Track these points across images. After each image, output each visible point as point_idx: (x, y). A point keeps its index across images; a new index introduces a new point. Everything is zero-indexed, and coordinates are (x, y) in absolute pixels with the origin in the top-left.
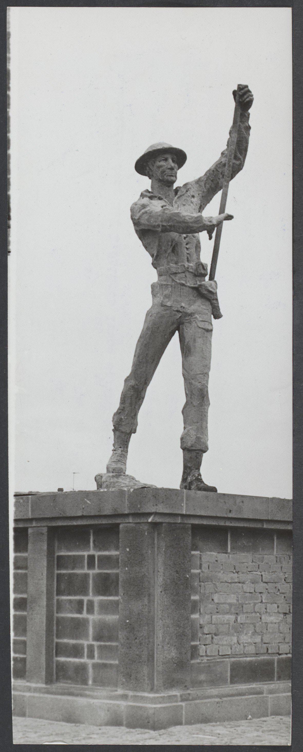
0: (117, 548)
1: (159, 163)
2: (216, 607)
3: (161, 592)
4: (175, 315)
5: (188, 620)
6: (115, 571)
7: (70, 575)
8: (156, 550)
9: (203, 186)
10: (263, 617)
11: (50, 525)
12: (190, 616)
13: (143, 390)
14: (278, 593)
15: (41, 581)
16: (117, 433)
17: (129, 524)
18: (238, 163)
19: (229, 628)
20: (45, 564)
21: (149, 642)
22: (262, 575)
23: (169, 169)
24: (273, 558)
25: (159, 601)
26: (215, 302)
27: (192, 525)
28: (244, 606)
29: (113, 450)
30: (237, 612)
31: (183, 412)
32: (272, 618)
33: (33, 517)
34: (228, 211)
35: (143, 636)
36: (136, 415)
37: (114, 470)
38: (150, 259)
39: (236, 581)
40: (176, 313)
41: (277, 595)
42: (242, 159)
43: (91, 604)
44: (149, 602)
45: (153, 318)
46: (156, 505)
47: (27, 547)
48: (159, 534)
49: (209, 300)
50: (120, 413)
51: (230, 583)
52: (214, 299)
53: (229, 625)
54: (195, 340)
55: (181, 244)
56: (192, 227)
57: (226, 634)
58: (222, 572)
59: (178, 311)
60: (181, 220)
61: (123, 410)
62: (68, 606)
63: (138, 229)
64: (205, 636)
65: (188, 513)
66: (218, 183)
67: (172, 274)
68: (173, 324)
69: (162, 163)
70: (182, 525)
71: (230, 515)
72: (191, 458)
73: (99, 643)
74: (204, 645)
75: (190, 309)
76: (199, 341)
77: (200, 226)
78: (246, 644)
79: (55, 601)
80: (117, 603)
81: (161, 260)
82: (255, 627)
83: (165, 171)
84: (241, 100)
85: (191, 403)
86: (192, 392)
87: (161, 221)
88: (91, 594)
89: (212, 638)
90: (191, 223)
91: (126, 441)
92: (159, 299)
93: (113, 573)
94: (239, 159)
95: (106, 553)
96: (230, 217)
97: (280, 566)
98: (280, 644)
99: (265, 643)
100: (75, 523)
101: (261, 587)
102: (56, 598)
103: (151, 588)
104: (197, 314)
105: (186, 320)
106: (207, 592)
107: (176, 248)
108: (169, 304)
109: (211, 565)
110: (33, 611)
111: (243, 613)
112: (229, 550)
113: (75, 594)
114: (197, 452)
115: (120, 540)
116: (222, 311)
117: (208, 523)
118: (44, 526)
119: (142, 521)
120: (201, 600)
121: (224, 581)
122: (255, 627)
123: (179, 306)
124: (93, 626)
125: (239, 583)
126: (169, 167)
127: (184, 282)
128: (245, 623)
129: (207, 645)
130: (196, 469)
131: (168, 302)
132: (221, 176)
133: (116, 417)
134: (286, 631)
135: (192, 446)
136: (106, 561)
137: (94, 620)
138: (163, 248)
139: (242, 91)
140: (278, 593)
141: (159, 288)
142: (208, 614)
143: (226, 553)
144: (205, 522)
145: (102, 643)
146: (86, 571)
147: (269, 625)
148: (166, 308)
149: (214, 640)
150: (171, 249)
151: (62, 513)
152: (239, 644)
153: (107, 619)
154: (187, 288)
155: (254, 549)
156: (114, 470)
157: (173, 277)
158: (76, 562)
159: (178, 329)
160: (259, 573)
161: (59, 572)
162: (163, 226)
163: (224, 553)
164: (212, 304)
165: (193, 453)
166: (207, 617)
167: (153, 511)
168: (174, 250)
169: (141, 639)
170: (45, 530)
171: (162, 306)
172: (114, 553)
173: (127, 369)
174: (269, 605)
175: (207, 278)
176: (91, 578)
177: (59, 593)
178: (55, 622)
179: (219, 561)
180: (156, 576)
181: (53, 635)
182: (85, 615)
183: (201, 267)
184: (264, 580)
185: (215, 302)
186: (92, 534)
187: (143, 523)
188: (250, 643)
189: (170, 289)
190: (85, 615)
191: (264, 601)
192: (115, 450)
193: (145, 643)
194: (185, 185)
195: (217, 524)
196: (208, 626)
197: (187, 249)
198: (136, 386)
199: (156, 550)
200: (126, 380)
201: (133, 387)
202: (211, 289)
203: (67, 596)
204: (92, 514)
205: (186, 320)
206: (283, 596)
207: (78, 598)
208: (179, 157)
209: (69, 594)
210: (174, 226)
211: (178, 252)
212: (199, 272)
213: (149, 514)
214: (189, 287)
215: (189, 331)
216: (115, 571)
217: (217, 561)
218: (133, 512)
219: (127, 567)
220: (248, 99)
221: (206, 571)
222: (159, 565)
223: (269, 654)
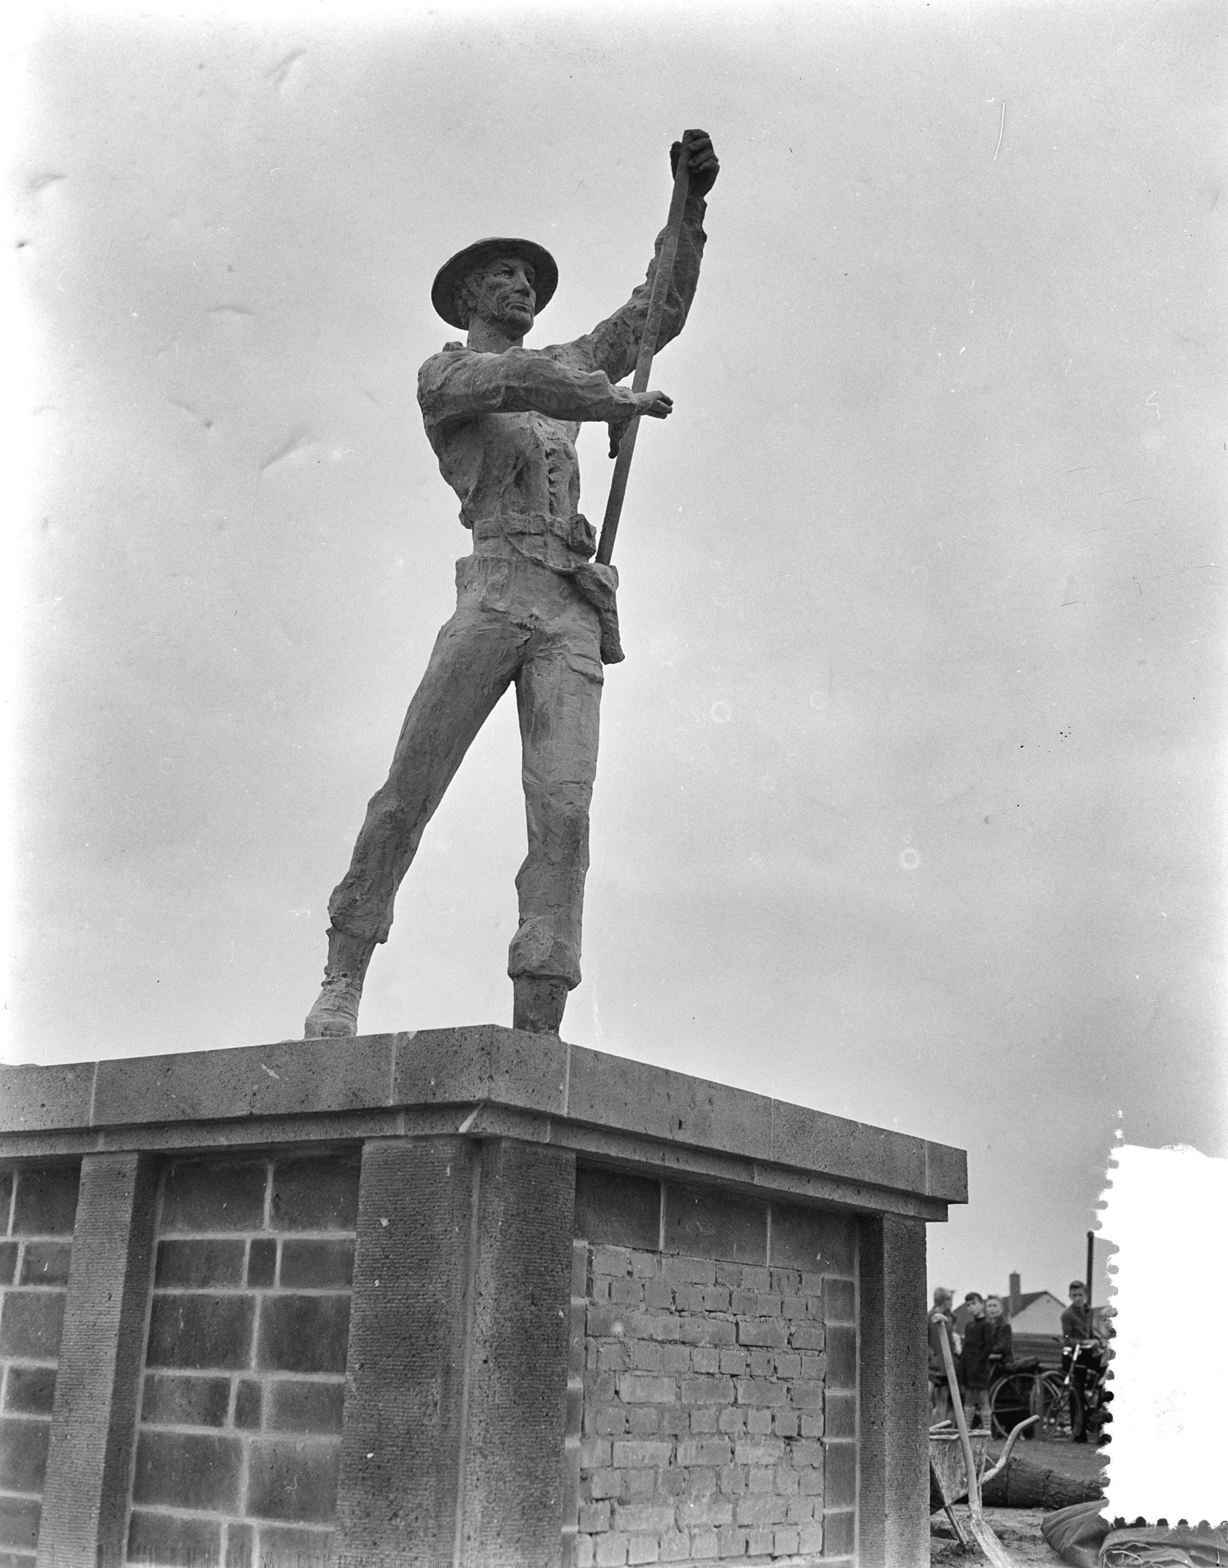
0: (347, 1221)
1: (492, 281)
2: (624, 1413)
3: (485, 1362)
4: (514, 635)
5: (557, 1454)
6: (333, 1292)
7: (193, 1299)
8: (474, 1226)
9: (591, 353)
10: (738, 1449)
11: (147, 1147)
12: (563, 1442)
13: (415, 825)
14: (774, 1379)
15: (104, 1319)
16: (340, 938)
17: (392, 1143)
18: (673, 311)
19: (656, 1480)
20: (122, 1265)
21: (440, 1526)
22: (737, 1324)
23: (517, 292)
24: (762, 1275)
25: (477, 1393)
26: (609, 616)
27: (582, 1156)
28: (695, 1414)
29: (323, 984)
30: (677, 1432)
31: (518, 883)
32: (760, 1451)
33: (98, 1123)
35: (420, 1505)
36: (391, 892)
37: (326, 1029)
38: (456, 505)
39: (677, 1337)
40: (518, 631)
41: (771, 1383)
42: (683, 305)
43: (250, 1394)
44: (445, 1396)
45: (458, 639)
46: (491, 1077)
47: (74, 1210)
48: (485, 1175)
49: (597, 610)
50: (352, 884)
51: (662, 1342)
52: (608, 610)
53: (657, 1473)
54: (560, 700)
55: (539, 467)
56: (582, 398)
57: (649, 1500)
58: (643, 1306)
59: (522, 626)
60: (556, 377)
61: (359, 878)
62: (178, 1399)
63: (433, 422)
64: (594, 1505)
65: (573, 1115)
66: (625, 352)
67: (511, 535)
68: (507, 657)
69: (503, 279)
70: (551, 1153)
71: (680, 1137)
72: (537, 997)
73: (268, 1523)
74: (591, 1534)
75: (551, 626)
76: (572, 702)
77: (602, 401)
78: (696, 1531)
79: (142, 1381)
80: (336, 1396)
81: (488, 499)
82: (719, 1477)
83: (507, 297)
84: (691, 163)
85: (545, 855)
86: (546, 827)
87: (506, 377)
88: (253, 1363)
89: (613, 1512)
90: (581, 387)
91: (361, 961)
92: (476, 594)
93: (328, 1298)
94: (677, 304)
95: (312, 1235)
96: (660, 408)
97: (778, 1299)
98: (776, 1528)
99: (740, 1527)
100: (223, 1140)
101: (734, 1359)
102: (145, 1372)
103: (455, 1350)
104: (569, 639)
105: (541, 651)
106: (604, 1367)
107: (525, 477)
108: (500, 606)
109: (616, 1285)
110: (71, 1411)
111: (692, 1436)
112: (661, 1246)
113: (204, 1363)
114: (552, 982)
115: (362, 1192)
116: (625, 644)
117: (621, 1155)
118: (128, 1152)
119: (436, 1132)
120: (587, 1394)
121: (644, 1336)
122: (719, 1477)
123: (525, 615)
124: (251, 1468)
125: (683, 1343)
126: (518, 287)
127: (540, 558)
128: (694, 1466)
129: (597, 1533)
130: (551, 1028)
131: (497, 600)
132: (632, 339)
133: (339, 897)
134: (789, 1491)
135: (542, 967)
136: (306, 1262)
137: (256, 1449)
138: (495, 473)
139: (697, 143)
140: (774, 1379)
141: (476, 567)
142: (603, 1437)
143: (654, 1252)
144: (614, 1150)
145: (279, 1524)
146: (242, 1290)
147: (753, 1471)
148: (492, 615)
149: (617, 1517)
150: (514, 475)
151: (189, 1110)
152: (680, 1531)
153: (299, 1447)
154: (548, 573)
155: (719, 1246)
156: (326, 1029)
157: (514, 541)
158: (216, 1262)
159: (516, 675)
160: (731, 1318)
161: (161, 1292)
162: (508, 388)
163: (648, 1251)
164: (602, 622)
165: (543, 982)
166: (601, 1446)
167: (480, 1095)
168: (519, 480)
169: (412, 1516)
170: (132, 1161)
171: (483, 610)
172: (334, 1234)
173: (379, 773)
174: (752, 1413)
176: (258, 1312)
177: (154, 1359)
178: (134, 1449)
179: (636, 1276)
180: (470, 1308)
181: (126, 1490)
182: (229, 1430)
183: (583, 528)
184: (742, 1338)
185: (609, 616)
186: (270, 1178)
187: (439, 1136)
188: (706, 1525)
189: (506, 571)
190: (229, 1430)
191: (740, 1401)
192: (329, 983)
193: (426, 1531)
195: (643, 1159)
196: (603, 1473)
197: (551, 482)
198: (400, 815)
199: (474, 1226)
200: (373, 803)
201: (391, 816)
202: (605, 582)
203: (181, 1367)
204: (282, 1110)
205: (541, 651)
206: (785, 1386)
207: (213, 1373)
209: (186, 1362)
210: (537, 391)
211: (528, 485)
212: (578, 540)
213: (464, 1108)
214: (553, 571)
215: (546, 679)
216: (333, 1292)
217: (630, 1273)
218: (411, 1100)
219: (380, 1278)
220: (707, 164)
221: (602, 1301)
222: (482, 1272)
223: (749, 1557)
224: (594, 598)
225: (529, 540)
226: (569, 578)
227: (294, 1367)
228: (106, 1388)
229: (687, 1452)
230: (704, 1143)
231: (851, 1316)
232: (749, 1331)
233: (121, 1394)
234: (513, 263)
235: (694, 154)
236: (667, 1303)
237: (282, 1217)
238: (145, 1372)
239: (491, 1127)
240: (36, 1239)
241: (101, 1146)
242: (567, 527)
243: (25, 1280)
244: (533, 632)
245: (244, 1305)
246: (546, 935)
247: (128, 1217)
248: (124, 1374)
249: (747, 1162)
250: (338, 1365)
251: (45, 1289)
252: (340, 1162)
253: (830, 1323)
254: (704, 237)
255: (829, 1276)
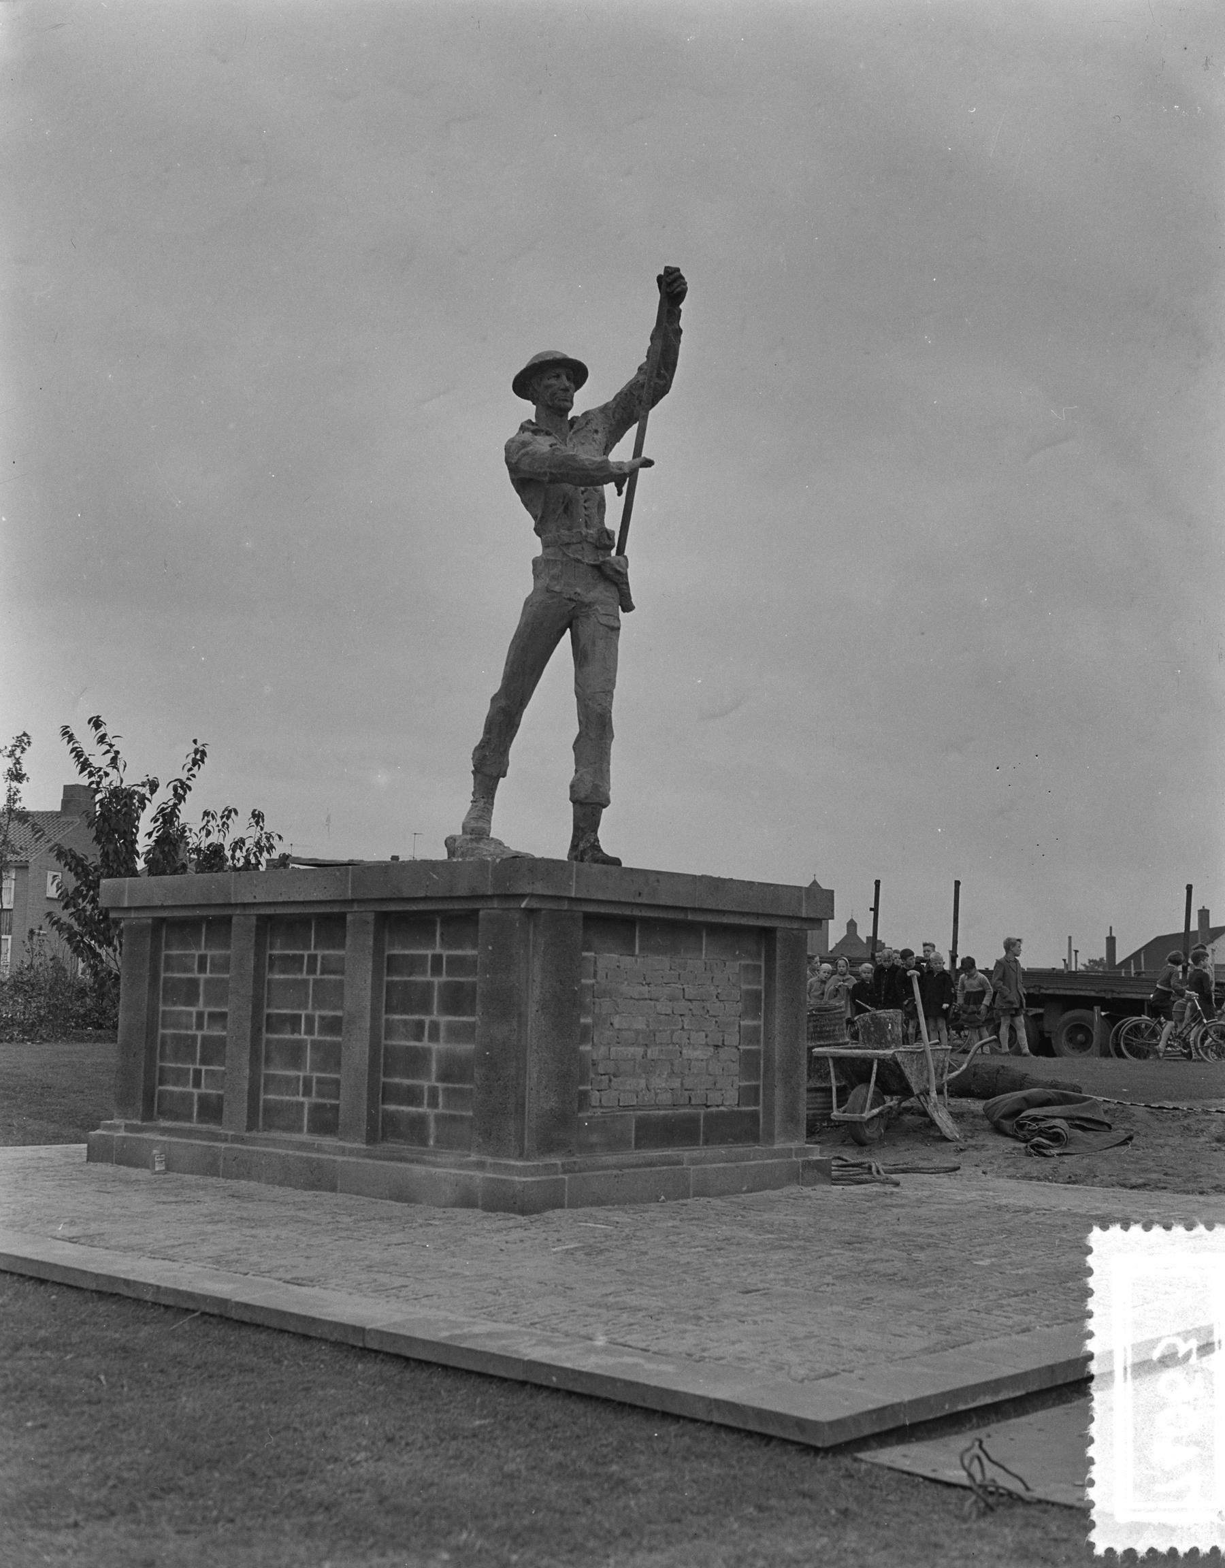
0: (475, 946)
6: (470, 979)
7: (405, 982)
10: (684, 1052)
16: (479, 776)
18: (662, 382)
20: (370, 965)
31: (574, 748)
34: (646, 454)
38: (532, 523)
43: (435, 1026)
48: (535, 926)
49: (616, 584)
54: (594, 643)
59: (570, 599)
69: (553, 381)
71: (639, 900)
73: (445, 1085)
76: (600, 644)
80: (472, 1026)
87: (549, 467)
89: (610, 1081)
95: (459, 952)
101: (682, 1006)
102: (384, 1017)
108: (557, 588)
112: (637, 951)
116: (634, 600)
136: (457, 964)
139: (672, 277)
144: (602, 910)
145: (450, 1085)
146: (428, 978)
158: (415, 964)
165: (588, 806)
166: (603, 1049)
168: (566, 510)
172: (470, 952)
175: (613, 552)
177: (389, 1010)
182: (425, 1043)
190: (425, 1043)
194: (586, 414)
200: (493, 700)
201: (503, 709)
204: (440, 895)
207: (416, 1017)
208: (577, 373)
209: (404, 1012)
212: (603, 541)
213: (523, 896)
215: (587, 629)
216: (470, 979)
224: (615, 580)
225: (573, 547)
226: (598, 568)
227: (454, 1014)
228: (367, 1023)
229: (653, 1052)
230: (654, 902)
231: (759, 983)
232: (691, 991)
233: (374, 1029)
234: (558, 371)
235: (669, 284)
236: (641, 980)
237: (446, 944)
238: (384, 1017)
239: (535, 904)
240: (327, 952)
241: (356, 908)
242: (596, 536)
243: (322, 973)
244: (579, 596)
245: (429, 985)
246: (588, 779)
247: (371, 943)
248: (375, 1018)
249: (684, 909)
250: (473, 1014)
251: (332, 977)
252: (470, 917)
253: (744, 987)
254: (681, 331)
255: (743, 962)
